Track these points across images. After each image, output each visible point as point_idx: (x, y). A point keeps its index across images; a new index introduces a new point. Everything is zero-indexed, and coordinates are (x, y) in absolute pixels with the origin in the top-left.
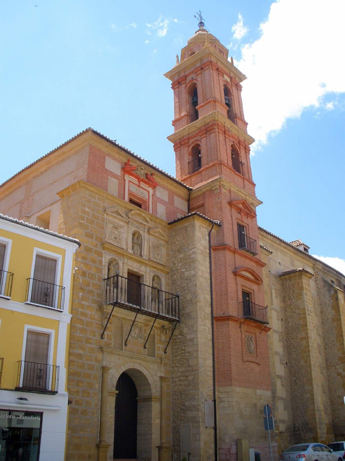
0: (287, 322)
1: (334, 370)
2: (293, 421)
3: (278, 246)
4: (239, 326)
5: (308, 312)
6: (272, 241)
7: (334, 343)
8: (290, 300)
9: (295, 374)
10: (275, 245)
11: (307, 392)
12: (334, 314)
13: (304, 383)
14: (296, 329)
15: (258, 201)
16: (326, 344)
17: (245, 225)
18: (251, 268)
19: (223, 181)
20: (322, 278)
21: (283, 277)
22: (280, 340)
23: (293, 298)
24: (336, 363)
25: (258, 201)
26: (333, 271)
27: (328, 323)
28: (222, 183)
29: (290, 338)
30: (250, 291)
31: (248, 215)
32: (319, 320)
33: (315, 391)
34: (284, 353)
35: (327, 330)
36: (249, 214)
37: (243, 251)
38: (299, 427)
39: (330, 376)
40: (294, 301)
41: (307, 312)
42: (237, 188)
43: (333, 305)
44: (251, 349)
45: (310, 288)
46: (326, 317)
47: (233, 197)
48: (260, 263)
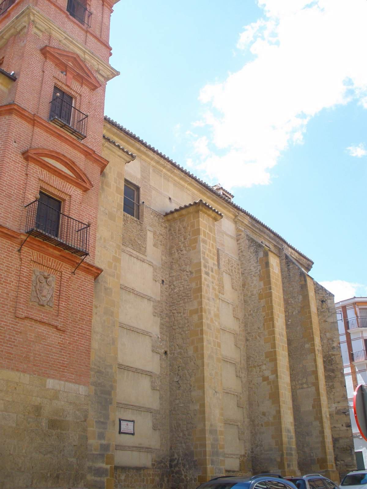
0: (172, 287)
1: (258, 372)
2: (171, 448)
3: (169, 174)
4: (17, 248)
5: (207, 270)
6: (158, 163)
7: (259, 331)
8: (179, 251)
9: (179, 370)
10: (164, 170)
11: (194, 402)
12: (263, 286)
13: (191, 385)
14: (184, 297)
15: (110, 69)
16: (248, 333)
17: (73, 93)
18: (66, 155)
19: (34, 14)
20: (247, 235)
21: (170, 217)
22: (156, 313)
23: (184, 249)
24: (262, 362)
25: (110, 69)
26: (268, 232)
27: (253, 301)
28: (32, 18)
29: (175, 311)
30: (63, 196)
31: (82, 79)
32: (239, 297)
33: (207, 400)
34: (161, 336)
35: (250, 311)
36: (85, 78)
37: (52, 123)
38: (179, 459)
39: (251, 381)
40: (184, 252)
41: (203, 269)
42: (66, 36)
43: (260, 273)
44: (44, 298)
45: (219, 238)
46: (251, 292)
47: (54, 44)
48: (93, 155)
